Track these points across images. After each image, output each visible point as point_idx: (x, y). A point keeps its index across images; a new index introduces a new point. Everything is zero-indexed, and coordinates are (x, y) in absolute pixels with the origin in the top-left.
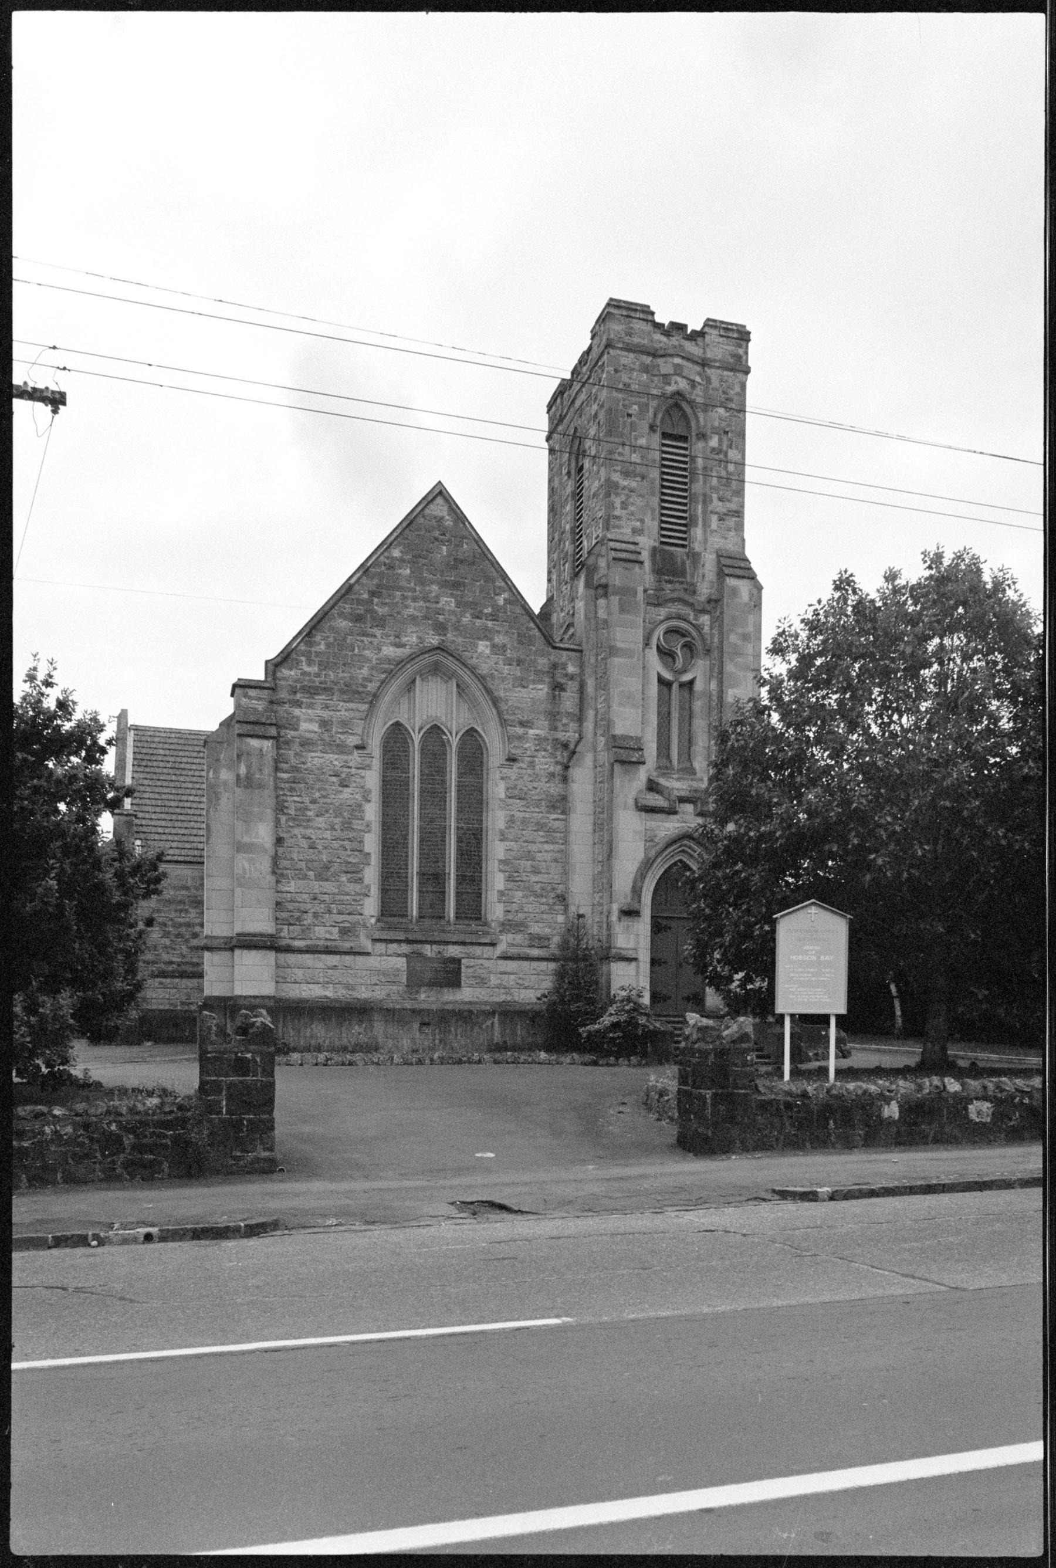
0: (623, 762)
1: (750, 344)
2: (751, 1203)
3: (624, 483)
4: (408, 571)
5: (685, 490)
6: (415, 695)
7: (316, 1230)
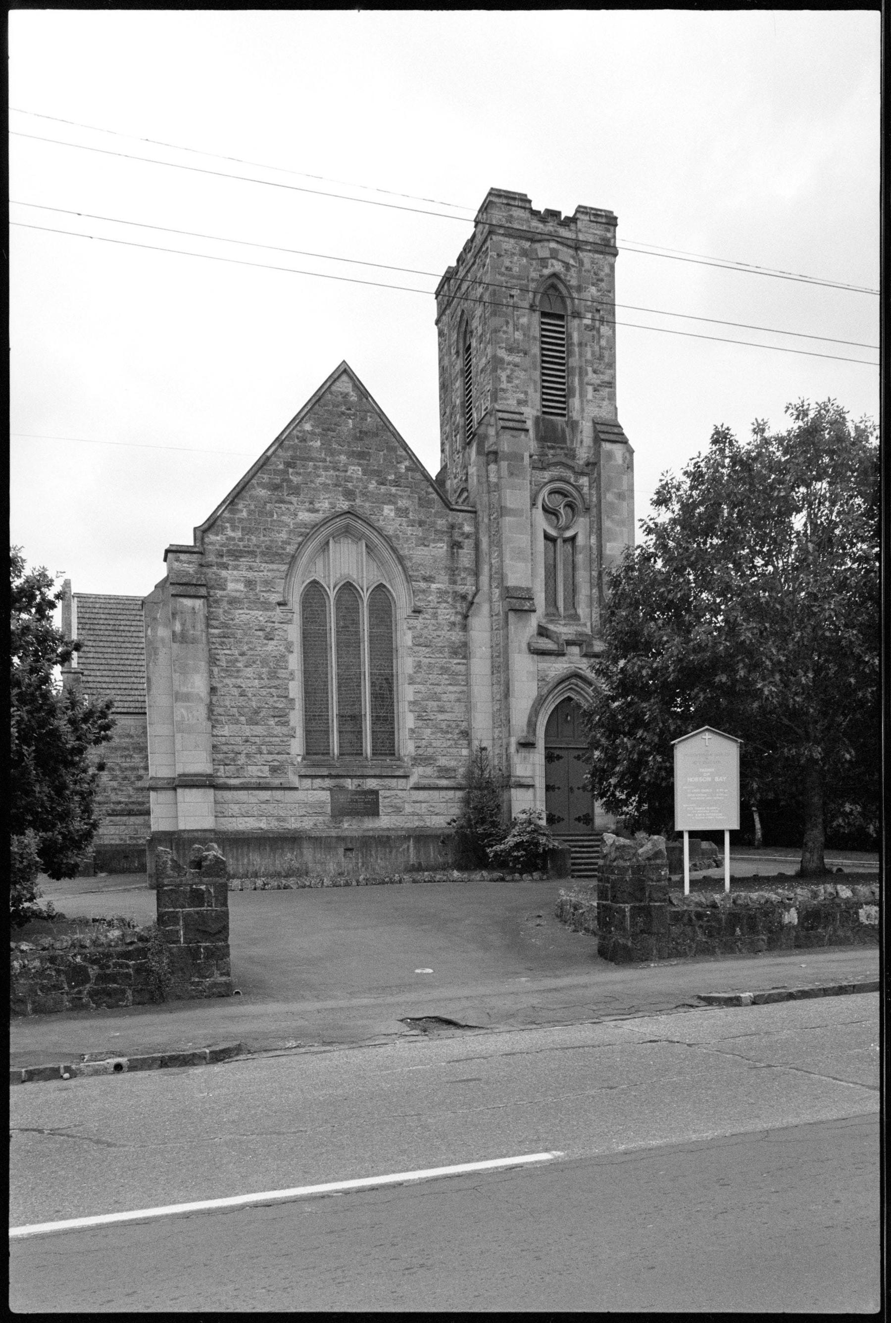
0: (516, 611)
1: (618, 228)
2: (680, 1009)
3: (508, 358)
4: (319, 443)
5: (563, 365)
6: (329, 558)
7: (278, 1053)
